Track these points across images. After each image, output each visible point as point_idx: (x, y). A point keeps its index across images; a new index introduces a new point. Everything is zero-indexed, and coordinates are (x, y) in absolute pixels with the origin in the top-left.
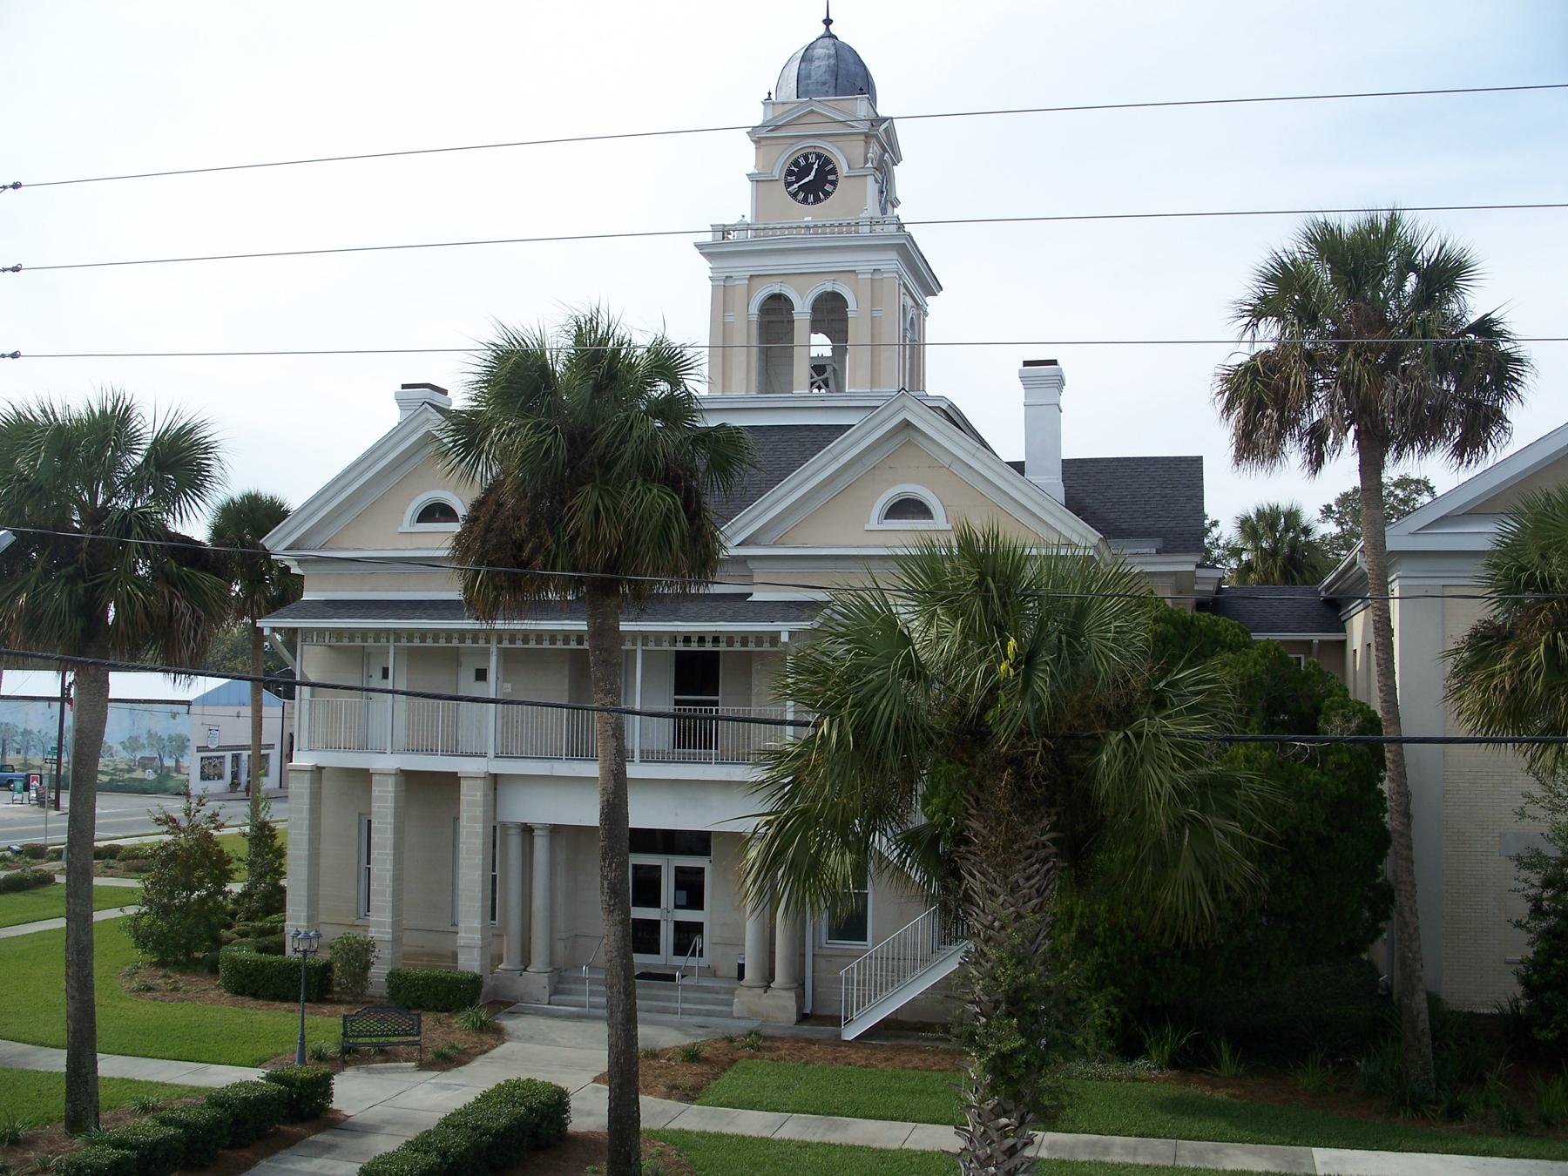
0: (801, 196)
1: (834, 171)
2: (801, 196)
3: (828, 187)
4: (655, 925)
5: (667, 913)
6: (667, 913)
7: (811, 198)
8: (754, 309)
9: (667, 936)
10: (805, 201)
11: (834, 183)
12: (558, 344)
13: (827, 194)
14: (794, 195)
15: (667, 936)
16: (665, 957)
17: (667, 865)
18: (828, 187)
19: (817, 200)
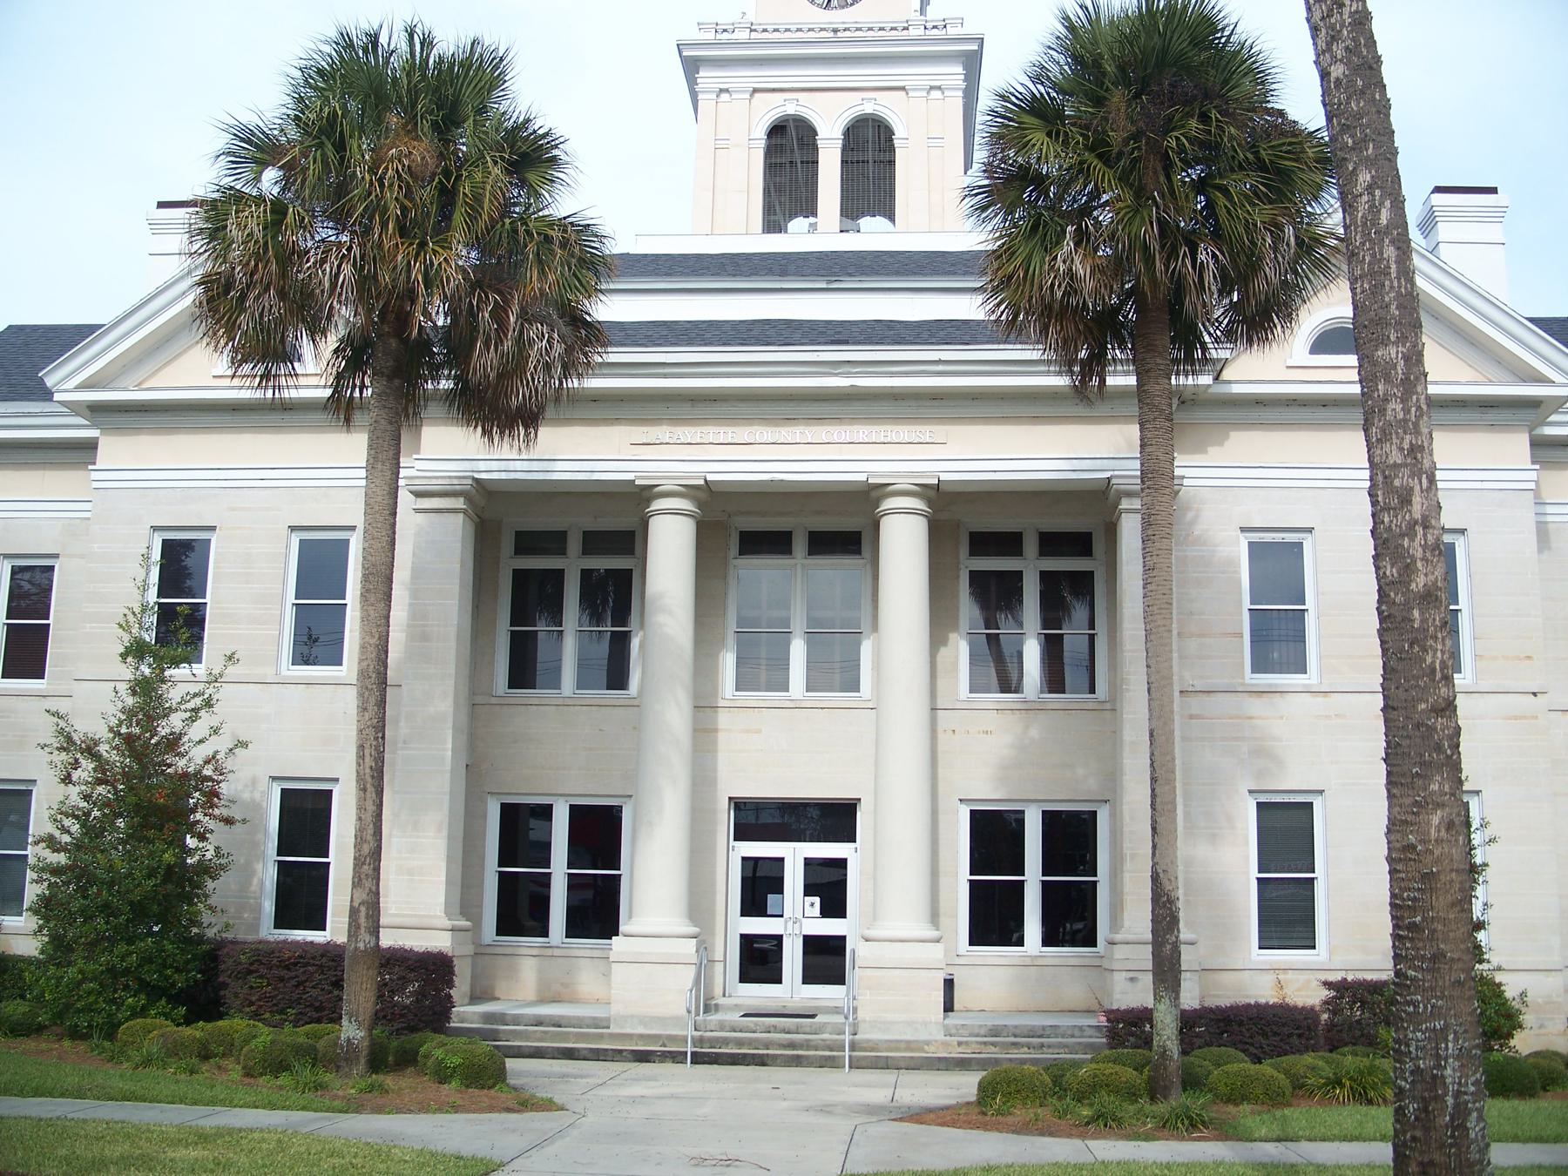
5: (796, 918)
6: (796, 918)
8: (761, 133)
9: (792, 959)
15: (792, 959)
17: (794, 855)
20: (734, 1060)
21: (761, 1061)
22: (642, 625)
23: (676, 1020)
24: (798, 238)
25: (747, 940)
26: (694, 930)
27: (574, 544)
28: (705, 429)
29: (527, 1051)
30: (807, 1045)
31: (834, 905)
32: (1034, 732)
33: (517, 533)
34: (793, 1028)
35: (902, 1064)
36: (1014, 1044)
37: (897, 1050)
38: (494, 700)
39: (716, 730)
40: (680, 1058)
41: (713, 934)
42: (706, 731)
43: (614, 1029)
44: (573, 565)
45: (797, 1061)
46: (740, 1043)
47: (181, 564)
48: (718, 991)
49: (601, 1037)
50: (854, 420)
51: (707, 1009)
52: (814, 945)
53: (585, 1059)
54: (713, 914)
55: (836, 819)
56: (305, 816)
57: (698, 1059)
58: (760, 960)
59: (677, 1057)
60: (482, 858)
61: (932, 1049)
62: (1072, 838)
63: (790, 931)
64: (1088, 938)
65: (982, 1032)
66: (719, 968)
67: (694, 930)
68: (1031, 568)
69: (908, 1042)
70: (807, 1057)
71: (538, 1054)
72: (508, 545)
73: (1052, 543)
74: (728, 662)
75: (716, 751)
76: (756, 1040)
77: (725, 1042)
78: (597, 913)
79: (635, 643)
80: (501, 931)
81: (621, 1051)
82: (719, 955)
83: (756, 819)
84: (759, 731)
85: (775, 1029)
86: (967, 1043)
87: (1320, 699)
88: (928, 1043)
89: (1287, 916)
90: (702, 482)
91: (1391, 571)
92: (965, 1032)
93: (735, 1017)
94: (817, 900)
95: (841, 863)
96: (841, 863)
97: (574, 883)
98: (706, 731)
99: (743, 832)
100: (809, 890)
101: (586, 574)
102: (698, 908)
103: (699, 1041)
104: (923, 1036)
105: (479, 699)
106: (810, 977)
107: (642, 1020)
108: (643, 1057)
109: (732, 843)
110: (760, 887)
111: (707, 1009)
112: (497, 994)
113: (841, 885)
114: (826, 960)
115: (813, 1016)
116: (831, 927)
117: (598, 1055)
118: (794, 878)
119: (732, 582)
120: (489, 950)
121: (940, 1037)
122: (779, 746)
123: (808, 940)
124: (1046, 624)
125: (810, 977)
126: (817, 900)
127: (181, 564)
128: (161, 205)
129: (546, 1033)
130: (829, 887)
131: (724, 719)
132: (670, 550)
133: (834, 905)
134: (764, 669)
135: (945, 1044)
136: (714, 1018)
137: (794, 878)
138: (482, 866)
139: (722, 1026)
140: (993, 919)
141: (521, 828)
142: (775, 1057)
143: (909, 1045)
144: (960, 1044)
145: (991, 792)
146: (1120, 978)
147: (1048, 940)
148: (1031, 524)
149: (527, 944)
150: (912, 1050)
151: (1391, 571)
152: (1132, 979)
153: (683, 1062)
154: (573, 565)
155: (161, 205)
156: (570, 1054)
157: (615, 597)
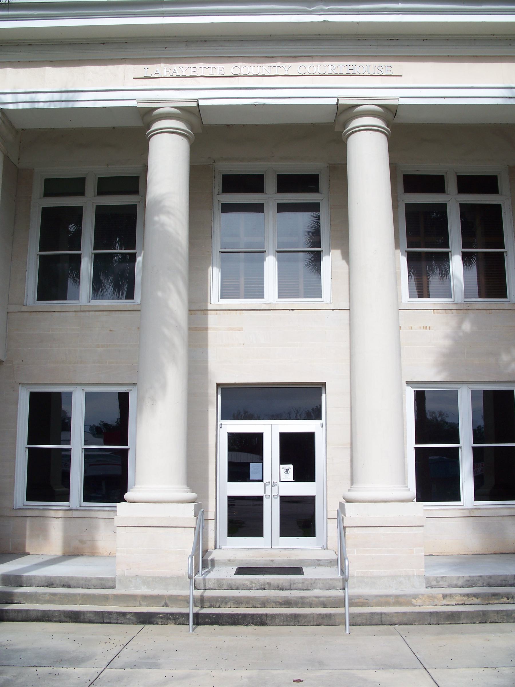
5: (274, 481)
6: (274, 481)
9: (271, 515)
15: (271, 515)
17: (271, 431)
20: (234, 620)
21: (260, 621)
22: (143, 248)
23: (176, 580)
25: (233, 502)
26: (192, 495)
27: (91, 187)
28: (198, 65)
29: (34, 615)
30: (302, 602)
31: (305, 471)
32: (467, 326)
33: (46, 180)
34: (287, 585)
35: (395, 620)
36: (495, 595)
37: (387, 604)
38: (24, 309)
39: (206, 329)
40: (181, 620)
41: (206, 497)
42: (196, 329)
43: (119, 590)
44: (90, 203)
45: (295, 620)
46: (238, 602)
48: (211, 545)
49: (105, 599)
50: (323, 58)
51: (205, 564)
52: (286, 502)
53: (91, 622)
54: (206, 479)
55: (305, 399)
57: (200, 620)
58: (244, 518)
59: (179, 619)
60: (14, 436)
61: (419, 602)
63: (268, 493)
65: (460, 583)
66: (211, 525)
67: (192, 495)
68: (453, 201)
69: (397, 596)
70: (304, 616)
71: (45, 617)
72: (38, 188)
73: (468, 184)
74: (215, 275)
75: (207, 346)
76: (254, 598)
77: (224, 601)
78: (109, 482)
79: (139, 259)
80: (30, 497)
81: (124, 614)
82: (211, 515)
83: (240, 400)
84: (241, 329)
85: (268, 586)
86: (451, 596)
88: (415, 597)
90: (195, 104)
92: (446, 584)
93: (228, 573)
94: (290, 467)
95: (310, 437)
96: (310, 437)
97: (90, 457)
98: (196, 329)
99: (228, 414)
100: (283, 460)
101: (99, 209)
102: (194, 476)
103: (201, 601)
104: (407, 590)
105: (12, 308)
106: (286, 531)
107: (147, 581)
108: (146, 619)
109: (220, 421)
110: (244, 452)
111: (205, 564)
112: (27, 550)
114: (299, 518)
115: (298, 571)
116: (302, 489)
117: (102, 618)
118: (271, 449)
119: (215, 226)
120: (20, 513)
121: (423, 590)
122: (259, 337)
123: (285, 501)
124: (465, 245)
125: (286, 531)
126: (290, 467)
129: (54, 594)
130: (299, 453)
131: (212, 319)
132: (168, 167)
133: (305, 471)
134: (245, 285)
135: (431, 597)
136: (214, 575)
137: (271, 449)
138: (14, 443)
139: (220, 585)
140: (435, 480)
142: (273, 617)
143: (398, 600)
144: (445, 596)
145: (429, 372)
149: (56, 507)
150: (400, 604)
153: (185, 623)
154: (90, 203)
156: (75, 617)
157: (122, 227)
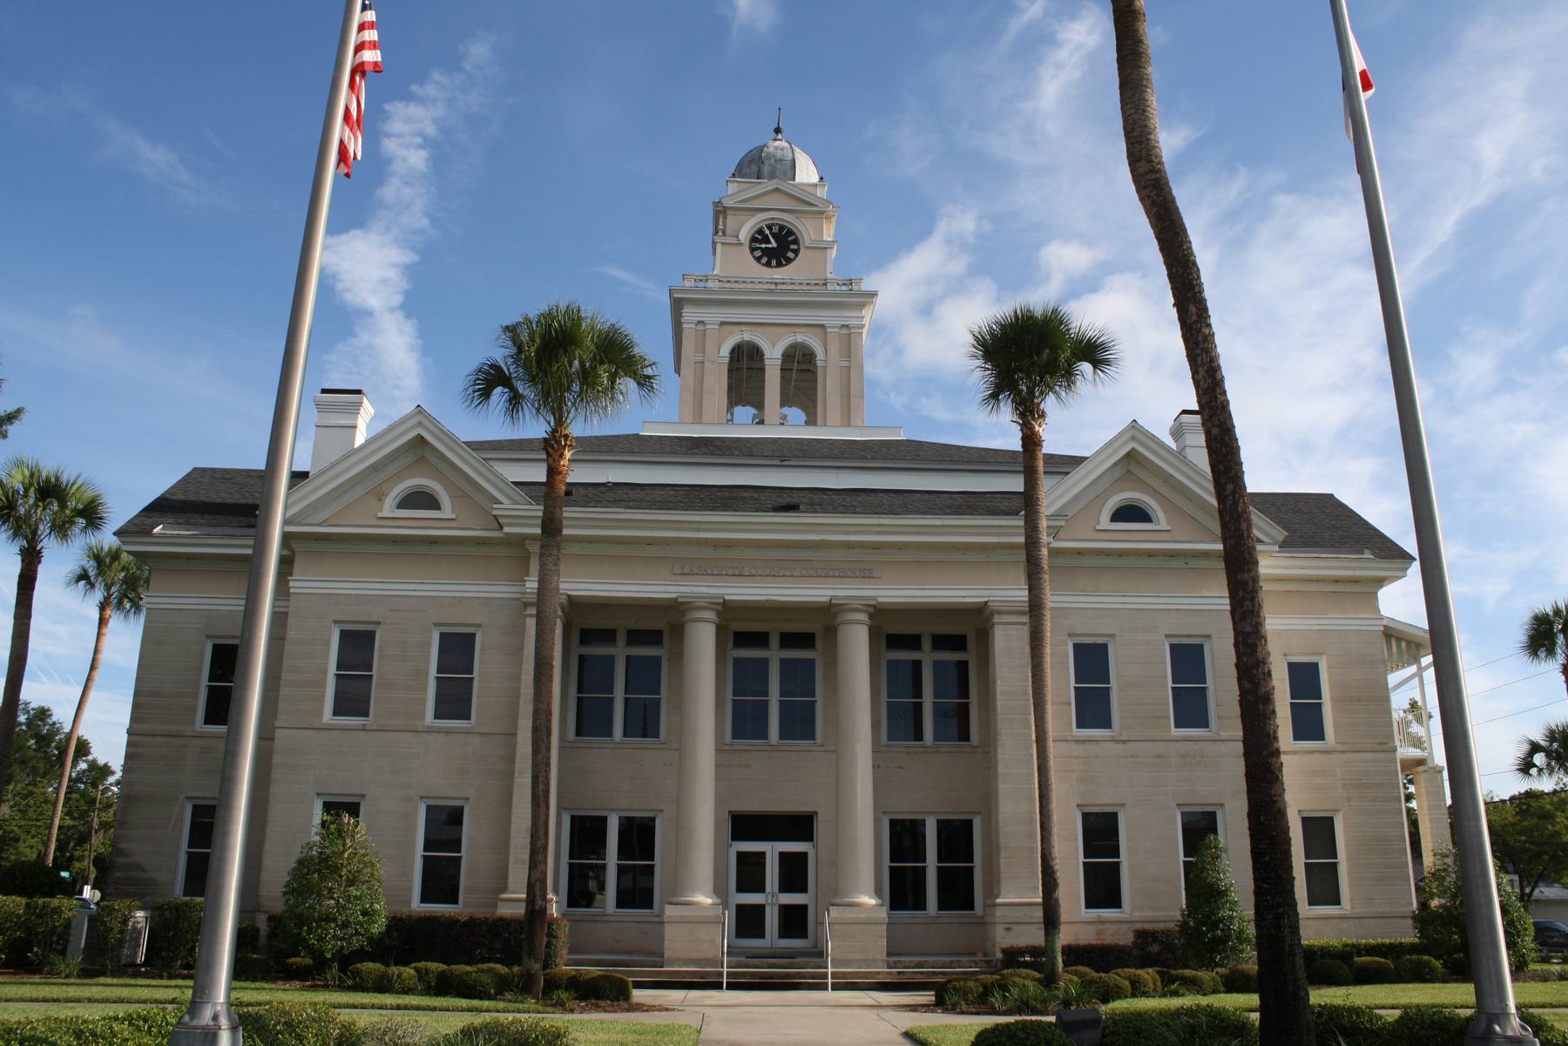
0: (758, 254)
1: (796, 242)
2: (758, 254)
3: (790, 255)
4: (760, 909)
5: (772, 898)
6: (772, 898)
7: (764, 260)
8: (725, 351)
9: (772, 920)
10: (758, 259)
11: (796, 252)
12: (563, 307)
13: (789, 261)
14: (752, 250)
15: (772, 920)
16: (772, 936)
17: (772, 850)
18: (790, 255)
19: (779, 265)
24: (743, 427)
47: (358, 645)
55: (800, 825)
56: (445, 825)
58: (749, 921)
62: (957, 837)
64: (969, 905)
83: (744, 825)
87: (1121, 746)
89: (1103, 887)
91: (1248, 686)
97: (601, 854)
110: (749, 873)
113: (1113, 833)
127: (358, 645)
128: (324, 391)
130: (794, 873)
141: (587, 833)
146: (1000, 929)
147: (941, 907)
148: (926, 629)
151: (1248, 686)
152: (1008, 929)
155: (324, 391)
